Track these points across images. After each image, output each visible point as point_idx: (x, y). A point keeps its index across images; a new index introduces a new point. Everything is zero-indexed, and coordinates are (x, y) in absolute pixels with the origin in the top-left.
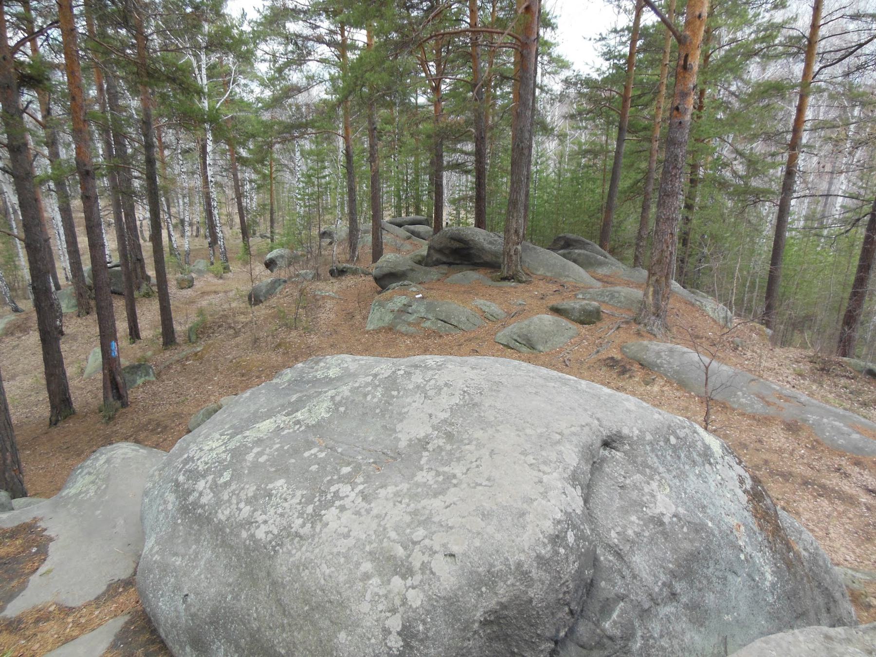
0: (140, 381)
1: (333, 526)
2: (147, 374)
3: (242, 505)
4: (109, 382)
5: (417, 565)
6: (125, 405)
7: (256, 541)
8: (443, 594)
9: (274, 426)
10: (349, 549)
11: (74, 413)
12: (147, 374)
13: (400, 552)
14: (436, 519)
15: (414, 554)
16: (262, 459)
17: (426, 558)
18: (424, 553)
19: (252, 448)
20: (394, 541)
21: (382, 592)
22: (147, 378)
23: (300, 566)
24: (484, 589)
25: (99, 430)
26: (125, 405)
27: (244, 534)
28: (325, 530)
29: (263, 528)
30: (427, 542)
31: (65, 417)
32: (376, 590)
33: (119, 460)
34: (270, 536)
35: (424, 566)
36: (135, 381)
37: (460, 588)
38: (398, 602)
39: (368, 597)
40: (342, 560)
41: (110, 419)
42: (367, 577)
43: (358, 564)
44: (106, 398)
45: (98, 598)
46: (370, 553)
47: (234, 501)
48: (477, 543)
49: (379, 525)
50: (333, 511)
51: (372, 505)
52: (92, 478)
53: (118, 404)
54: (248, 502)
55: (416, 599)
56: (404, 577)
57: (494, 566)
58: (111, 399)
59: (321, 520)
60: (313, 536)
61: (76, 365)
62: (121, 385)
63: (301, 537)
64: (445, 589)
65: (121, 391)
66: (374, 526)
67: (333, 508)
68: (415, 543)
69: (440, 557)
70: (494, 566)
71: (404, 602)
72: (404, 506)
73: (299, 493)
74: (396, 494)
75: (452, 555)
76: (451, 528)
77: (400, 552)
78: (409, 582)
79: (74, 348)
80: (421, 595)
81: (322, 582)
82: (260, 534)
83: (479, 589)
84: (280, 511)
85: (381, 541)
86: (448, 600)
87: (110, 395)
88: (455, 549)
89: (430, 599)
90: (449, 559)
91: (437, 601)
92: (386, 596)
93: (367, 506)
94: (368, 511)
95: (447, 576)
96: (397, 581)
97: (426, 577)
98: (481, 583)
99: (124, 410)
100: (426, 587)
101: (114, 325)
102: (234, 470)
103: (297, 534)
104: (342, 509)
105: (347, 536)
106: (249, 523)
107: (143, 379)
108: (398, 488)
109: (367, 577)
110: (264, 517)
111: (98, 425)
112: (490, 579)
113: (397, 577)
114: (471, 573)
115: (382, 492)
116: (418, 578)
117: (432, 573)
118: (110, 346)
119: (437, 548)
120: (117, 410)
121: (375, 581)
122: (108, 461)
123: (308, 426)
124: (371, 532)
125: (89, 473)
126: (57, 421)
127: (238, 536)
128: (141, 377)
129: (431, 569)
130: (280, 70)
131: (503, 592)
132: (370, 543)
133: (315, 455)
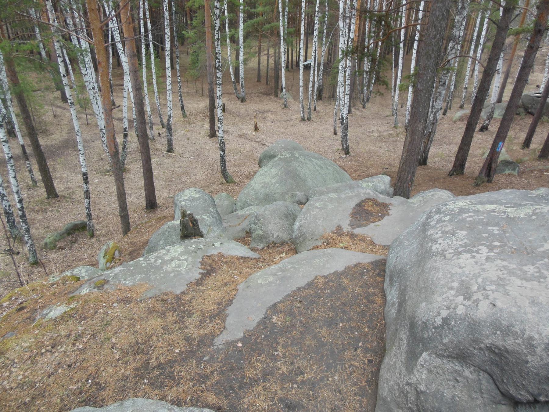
0: (507, 172)
1: (461, 261)
2: (514, 170)
3: (439, 232)
4: (487, 164)
5: (475, 297)
6: (489, 181)
7: (431, 249)
8: (473, 317)
9: (493, 208)
10: (456, 273)
11: (463, 174)
12: (514, 170)
13: (475, 288)
14: (507, 287)
15: (478, 293)
16: (468, 219)
17: (481, 298)
18: (483, 295)
19: (470, 212)
20: (477, 283)
21: (451, 298)
22: (513, 172)
23: (436, 269)
24: (498, 332)
25: (468, 188)
26: (489, 181)
27: (430, 244)
28: (456, 260)
29: (437, 246)
30: (490, 293)
31: (457, 174)
32: (450, 296)
33: (437, 197)
34: (437, 250)
35: (477, 301)
36: (504, 171)
37: (484, 321)
38: (453, 306)
39: (444, 296)
40: (449, 276)
41: (478, 185)
42: (451, 288)
43: (454, 281)
44: (481, 173)
45: (385, 246)
46: (462, 281)
47: (439, 229)
48: (514, 310)
49: (479, 273)
50: (469, 255)
51: (487, 264)
52: (422, 199)
53: (486, 179)
54: (443, 233)
55: (461, 310)
56: (465, 299)
57: (514, 327)
58: (483, 175)
59: (459, 255)
60: (449, 260)
61: (482, 150)
62: (493, 169)
63: (445, 257)
64: (477, 316)
65: (492, 173)
66: (476, 272)
67: (470, 255)
68: (484, 289)
69: (488, 302)
70: (514, 327)
71: (455, 308)
72: (501, 273)
73: (465, 241)
74: (504, 267)
75: (494, 305)
76: (508, 295)
77: (475, 288)
78: (465, 302)
79: (488, 140)
80: (464, 311)
81: (435, 279)
82: (434, 248)
83: (496, 330)
84: (450, 243)
85: (472, 279)
86: (474, 321)
87: (484, 172)
88: (499, 304)
89: (466, 315)
90: (491, 306)
91: (468, 318)
92: (451, 301)
93: (484, 262)
94: (482, 265)
95: (483, 311)
96: (461, 298)
97: (473, 305)
98: (499, 328)
99: (487, 184)
100: (469, 309)
101: (507, 132)
102: (452, 217)
103: (445, 256)
104: (473, 257)
105: (461, 268)
106: (435, 241)
107: (510, 172)
108: (509, 265)
109: (451, 288)
110: (442, 242)
111: (469, 186)
112: (507, 331)
113: (462, 297)
114: (496, 320)
115: (499, 261)
116: (470, 303)
117: (477, 306)
118: (498, 144)
119: (490, 297)
120: (483, 182)
121: (453, 292)
122: (432, 195)
123: (507, 217)
124: (472, 273)
125: (423, 197)
126: (453, 174)
127: (427, 243)
128: (509, 170)
129: (478, 303)
130: (85, 63)
131: (509, 343)
132: (467, 277)
133: (493, 230)
